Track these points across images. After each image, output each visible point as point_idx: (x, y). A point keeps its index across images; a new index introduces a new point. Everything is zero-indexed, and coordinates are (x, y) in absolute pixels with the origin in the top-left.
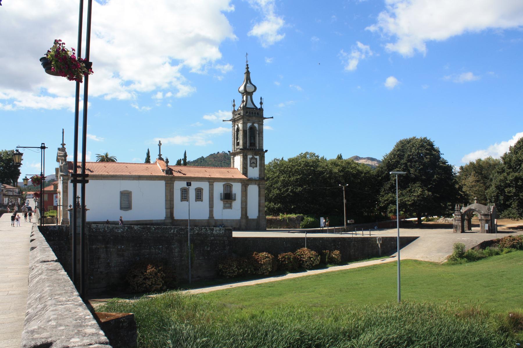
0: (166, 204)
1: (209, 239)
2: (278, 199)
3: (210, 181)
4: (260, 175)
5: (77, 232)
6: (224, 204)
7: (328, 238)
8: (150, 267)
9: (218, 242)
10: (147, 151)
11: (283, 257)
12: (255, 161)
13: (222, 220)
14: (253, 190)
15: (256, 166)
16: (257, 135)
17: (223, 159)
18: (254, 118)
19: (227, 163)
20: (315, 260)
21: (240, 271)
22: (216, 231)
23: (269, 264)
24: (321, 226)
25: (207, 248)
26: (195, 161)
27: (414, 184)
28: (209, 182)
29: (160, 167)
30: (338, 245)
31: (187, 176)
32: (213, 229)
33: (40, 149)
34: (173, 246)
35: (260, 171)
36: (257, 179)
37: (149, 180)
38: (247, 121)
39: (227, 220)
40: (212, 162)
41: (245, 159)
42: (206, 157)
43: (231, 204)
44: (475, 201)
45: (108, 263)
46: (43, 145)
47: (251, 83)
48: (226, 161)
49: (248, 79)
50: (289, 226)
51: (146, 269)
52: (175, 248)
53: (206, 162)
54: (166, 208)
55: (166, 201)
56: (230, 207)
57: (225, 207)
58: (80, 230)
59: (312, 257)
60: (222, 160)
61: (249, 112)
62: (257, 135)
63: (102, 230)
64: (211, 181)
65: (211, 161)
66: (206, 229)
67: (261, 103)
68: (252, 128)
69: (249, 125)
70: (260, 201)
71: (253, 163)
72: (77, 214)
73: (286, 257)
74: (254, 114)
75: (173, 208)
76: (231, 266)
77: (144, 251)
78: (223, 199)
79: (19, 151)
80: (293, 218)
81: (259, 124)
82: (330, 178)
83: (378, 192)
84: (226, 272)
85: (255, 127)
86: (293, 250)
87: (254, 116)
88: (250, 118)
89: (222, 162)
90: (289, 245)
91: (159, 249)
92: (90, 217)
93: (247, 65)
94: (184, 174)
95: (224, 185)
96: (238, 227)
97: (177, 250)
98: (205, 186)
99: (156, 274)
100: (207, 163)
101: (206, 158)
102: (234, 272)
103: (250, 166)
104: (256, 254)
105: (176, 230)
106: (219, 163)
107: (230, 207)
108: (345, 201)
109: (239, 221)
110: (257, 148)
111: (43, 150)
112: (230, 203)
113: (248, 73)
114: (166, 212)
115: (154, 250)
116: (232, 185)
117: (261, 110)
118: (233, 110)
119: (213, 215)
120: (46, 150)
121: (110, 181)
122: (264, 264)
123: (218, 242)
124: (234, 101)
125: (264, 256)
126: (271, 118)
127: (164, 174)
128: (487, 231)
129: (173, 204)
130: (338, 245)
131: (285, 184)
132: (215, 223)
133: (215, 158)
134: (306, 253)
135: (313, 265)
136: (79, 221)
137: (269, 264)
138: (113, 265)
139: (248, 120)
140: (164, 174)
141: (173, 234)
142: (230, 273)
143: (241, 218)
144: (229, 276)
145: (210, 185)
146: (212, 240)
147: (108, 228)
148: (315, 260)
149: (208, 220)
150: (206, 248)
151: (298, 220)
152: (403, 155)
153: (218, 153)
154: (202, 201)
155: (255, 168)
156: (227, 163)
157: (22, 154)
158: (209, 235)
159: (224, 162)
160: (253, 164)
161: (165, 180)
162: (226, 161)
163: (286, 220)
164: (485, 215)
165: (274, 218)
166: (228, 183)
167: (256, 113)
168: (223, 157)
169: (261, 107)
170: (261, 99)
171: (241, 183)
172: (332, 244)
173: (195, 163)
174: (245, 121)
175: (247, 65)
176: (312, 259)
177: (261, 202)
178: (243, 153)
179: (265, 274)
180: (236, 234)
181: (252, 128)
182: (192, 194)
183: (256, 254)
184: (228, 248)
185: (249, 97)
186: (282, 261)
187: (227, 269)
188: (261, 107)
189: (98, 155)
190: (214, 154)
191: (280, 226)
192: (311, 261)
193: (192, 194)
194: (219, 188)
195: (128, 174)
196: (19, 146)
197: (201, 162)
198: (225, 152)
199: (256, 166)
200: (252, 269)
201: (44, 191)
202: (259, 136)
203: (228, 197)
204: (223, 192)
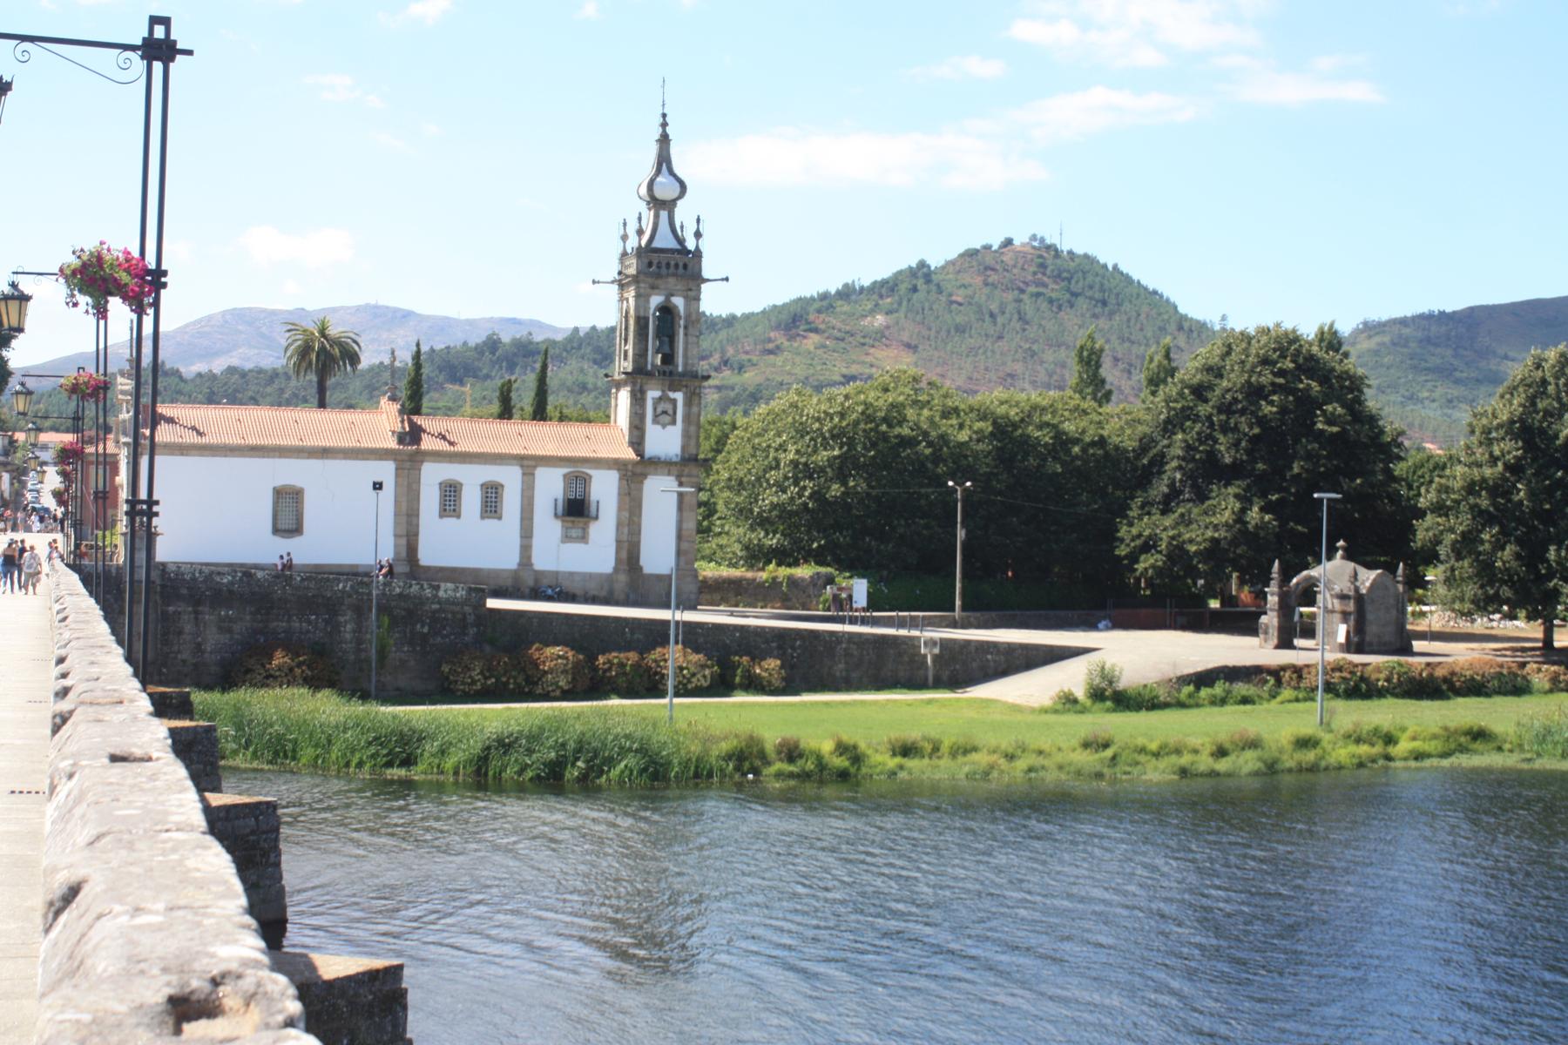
0: (396, 524)
1: (427, 608)
2: (783, 517)
3: (526, 463)
4: (684, 448)
5: (136, 577)
6: (566, 529)
7: (763, 628)
8: (279, 654)
9: (450, 616)
10: (415, 349)
11: (609, 661)
12: (669, 407)
13: (557, 573)
14: (661, 495)
15: (674, 422)
16: (681, 331)
17: (1030, 278)
18: (672, 280)
19: (1051, 301)
20: (694, 675)
21: (489, 682)
22: (446, 591)
23: (565, 672)
24: (855, 606)
25: (423, 626)
26: (884, 283)
27: (1226, 486)
28: (522, 466)
29: (387, 425)
30: (794, 648)
31: (457, 449)
32: (439, 587)
33: (137, 62)
34: (342, 619)
35: (686, 435)
36: (674, 459)
37: (350, 458)
38: (649, 290)
39: (571, 574)
40: (969, 292)
41: (638, 399)
42: (942, 263)
43: (585, 530)
44: (1340, 553)
45: (199, 645)
46: (159, 32)
47: (671, 172)
48: (1045, 285)
49: (664, 160)
50: (789, 604)
51: (271, 658)
52: (346, 622)
53: (940, 290)
54: (396, 536)
55: (396, 515)
56: (584, 538)
57: (567, 538)
58: (142, 574)
59: (687, 668)
60: (1026, 284)
61: (655, 262)
62: (681, 331)
63: (187, 577)
64: (529, 464)
65: (964, 286)
66: (422, 586)
67: (698, 235)
68: (667, 311)
69: (656, 300)
70: (680, 523)
71: (665, 412)
72: (137, 540)
73: (616, 661)
74: (672, 270)
75: (417, 534)
76: (469, 669)
77: (275, 624)
78: (563, 515)
79: (20, 287)
80: (803, 579)
81: (686, 298)
82: (937, 458)
83: (1121, 510)
84: (456, 682)
85: (676, 307)
86: (644, 649)
87: (675, 275)
88: (659, 282)
89: (1022, 291)
90: (641, 637)
91: (309, 622)
92: (165, 551)
93: (664, 116)
94: (451, 444)
95: (565, 476)
96: (603, 593)
97: (349, 627)
98: (510, 478)
99: (291, 670)
100: (943, 299)
101: (943, 268)
102: (474, 682)
103: (656, 420)
104: (537, 649)
105: (349, 583)
106: (1010, 296)
107: (584, 538)
108: (961, 534)
109: (515, 574)
110: (680, 369)
111: (158, 66)
112: (581, 525)
113: (664, 140)
114: (396, 546)
115: (297, 625)
116: (590, 477)
117: (698, 254)
118: (620, 250)
119: (529, 558)
120: (179, 64)
121: (247, 460)
122: (551, 671)
123: (450, 616)
124: (698, 221)
125: (554, 656)
126: (722, 280)
127: (392, 444)
128: (1341, 645)
129: (418, 526)
130: (794, 648)
131: (803, 471)
132: (536, 581)
133: (987, 268)
134: (674, 656)
135: (689, 686)
136: (141, 556)
137: (565, 672)
138: (209, 649)
139: (653, 287)
140: (392, 444)
141: (343, 591)
142: (463, 683)
143: (616, 569)
144: (463, 691)
145: (524, 474)
146: (434, 612)
147: (200, 572)
148: (694, 675)
149: (516, 572)
150: (418, 626)
151: (815, 585)
152: (1211, 387)
153: (1008, 242)
154: (500, 518)
155: (669, 428)
156: (1051, 301)
157: (27, 298)
158: (428, 599)
159: (1038, 295)
160: (665, 416)
161: (395, 460)
162: (1045, 285)
163: (781, 583)
164: (1343, 597)
165: (750, 575)
166: (578, 472)
167: (681, 265)
168: (1033, 269)
169: (697, 247)
170: (698, 221)
171: (618, 470)
172: (774, 645)
173: (881, 297)
174: (642, 291)
175: (664, 116)
176: (685, 672)
177: (685, 526)
178: (634, 384)
179: (552, 694)
180: (492, 603)
181: (667, 311)
182: (471, 500)
183: (537, 649)
184: (472, 631)
185: (664, 214)
186: (605, 671)
187: (459, 673)
188: (697, 247)
189: (290, 327)
190: (987, 248)
191: (764, 600)
192: (684, 676)
193: (471, 500)
194: (551, 486)
195: (297, 443)
196: (20, 270)
197: (915, 289)
198: (1042, 240)
199: (674, 422)
200: (520, 679)
201: (105, 454)
202: (686, 335)
203: (576, 509)
204: (560, 497)
